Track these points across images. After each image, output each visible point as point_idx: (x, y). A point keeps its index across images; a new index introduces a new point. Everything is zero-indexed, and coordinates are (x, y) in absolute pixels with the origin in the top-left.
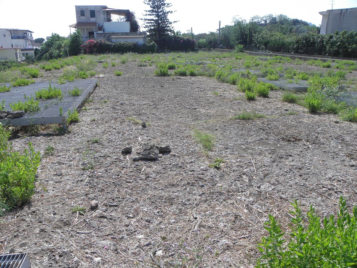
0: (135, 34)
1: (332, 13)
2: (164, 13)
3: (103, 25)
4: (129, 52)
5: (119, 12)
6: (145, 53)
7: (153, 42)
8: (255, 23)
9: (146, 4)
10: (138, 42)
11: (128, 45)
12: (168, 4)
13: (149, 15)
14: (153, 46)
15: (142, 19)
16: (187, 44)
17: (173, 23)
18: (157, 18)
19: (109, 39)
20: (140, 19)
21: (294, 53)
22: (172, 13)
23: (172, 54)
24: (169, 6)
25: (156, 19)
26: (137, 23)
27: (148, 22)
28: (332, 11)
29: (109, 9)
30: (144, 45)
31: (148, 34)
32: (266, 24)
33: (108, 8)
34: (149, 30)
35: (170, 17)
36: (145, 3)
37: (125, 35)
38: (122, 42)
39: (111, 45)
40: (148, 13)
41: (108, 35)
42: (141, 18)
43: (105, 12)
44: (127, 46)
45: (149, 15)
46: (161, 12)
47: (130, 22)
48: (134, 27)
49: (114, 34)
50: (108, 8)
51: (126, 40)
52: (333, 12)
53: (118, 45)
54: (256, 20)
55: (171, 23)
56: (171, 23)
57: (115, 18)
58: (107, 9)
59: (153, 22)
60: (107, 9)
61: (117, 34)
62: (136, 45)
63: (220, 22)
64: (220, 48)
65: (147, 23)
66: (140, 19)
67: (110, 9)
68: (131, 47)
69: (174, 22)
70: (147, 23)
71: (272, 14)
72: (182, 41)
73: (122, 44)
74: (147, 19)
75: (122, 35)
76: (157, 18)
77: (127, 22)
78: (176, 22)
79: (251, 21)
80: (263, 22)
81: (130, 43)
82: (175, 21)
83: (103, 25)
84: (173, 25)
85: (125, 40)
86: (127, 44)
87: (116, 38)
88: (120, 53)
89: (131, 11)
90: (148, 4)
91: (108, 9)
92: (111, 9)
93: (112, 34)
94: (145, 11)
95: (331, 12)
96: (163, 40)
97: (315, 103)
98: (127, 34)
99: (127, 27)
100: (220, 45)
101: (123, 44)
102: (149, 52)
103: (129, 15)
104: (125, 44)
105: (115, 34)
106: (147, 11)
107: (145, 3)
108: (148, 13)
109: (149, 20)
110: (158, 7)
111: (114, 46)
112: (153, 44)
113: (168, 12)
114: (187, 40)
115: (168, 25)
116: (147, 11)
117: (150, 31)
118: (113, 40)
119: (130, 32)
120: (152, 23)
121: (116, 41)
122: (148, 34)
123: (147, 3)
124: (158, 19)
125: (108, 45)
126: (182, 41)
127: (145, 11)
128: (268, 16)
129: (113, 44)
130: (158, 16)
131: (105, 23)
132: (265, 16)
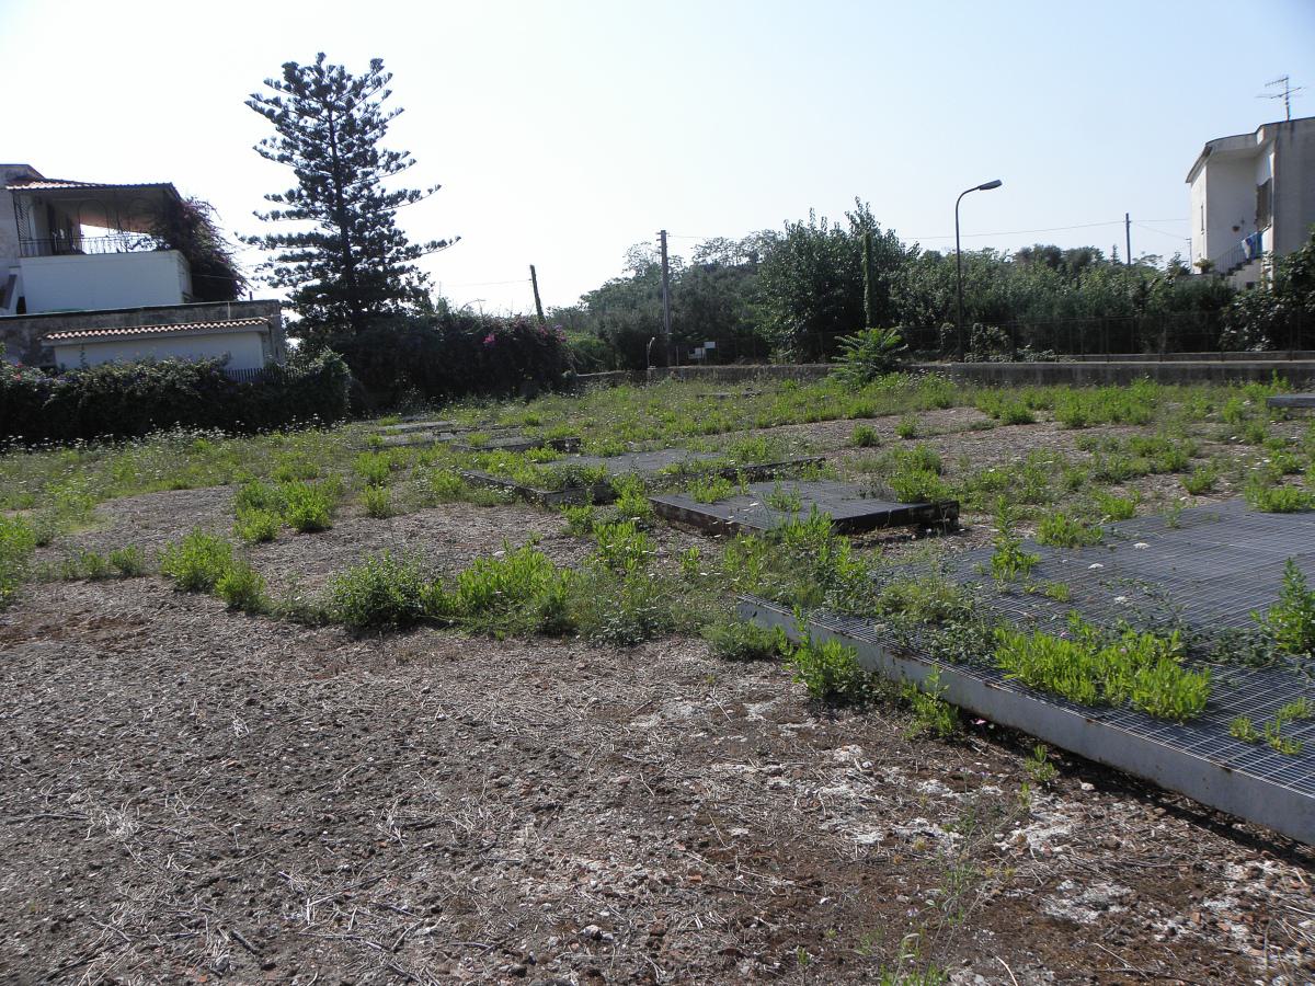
0: (212, 312)
1: (1292, 138)
2: (374, 203)
3: (13, 278)
4: (167, 426)
5: (117, 204)
6: (274, 427)
7: (327, 352)
8: (715, 266)
9: (272, 158)
10: (227, 358)
11: (157, 380)
12: (394, 157)
13: (290, 214)
14: (329, 374)
15: (253, 241)
16: (508, 360)
17: (424, 250)
18: (337, 230)
19: (38, 355)
20: (242, 239)
21: (1269, 347)
22: (417, 203)
23: (462, 417)
24: (399, 167)
25: (331, 233)
26: (228, 261)
27: (288, 252)
28: (1292, 129)
29: (50, 186)
30: (271, 377)
31: (294, 316)
32: (751, 268)
33: (46, 181)
34: (295, 298)
35: (405, 219)
36: (265, 155)
37: (146, 323)
38: (122, 363)
39: (44, 390)
40: (284, 207)
41: (33, 326)
42: (249, 235)
43: (26, 202)
44: (151, 389)
45: (290, 214)
46: (355, 198)
47: (186, 253)
48: (212, 278)
49: (70, 318)
50: (46, 181)
51: (151, 350)
52: (1300, 132)
53: (89, 388)
54: (719, 254)
55: (414, 252)
56: (414, 252)
57: (96, 238)
58: (34, 186)
59: (314, 250)
60: (34, 186)
61: (94, 318)
62: (214, 380)
63: (663, 233)
64: (703, 364)
65: (284, 259)
66: (242, 239)
67: (53, 181)
68: (183, 392)
69: (434, 245)
70: (284, 259)
71: (771, 229)
72: (490, 338)
73: (116, 380)
74: (281, 240)
75: (128, 325)
76: (337, 230)
77: (161, 253)
78: (443, 244)
79: (700, 260)
80: (745, 260)
81: (173, 367)
82: (438, 240)
83: (13, 278)
84: (422, 263)
85: (143, 352)
86: (151, 378)
87: (81, 345)
88: (106, 442)
89: (185, 193)
90: (282, 159)
91: (42, 186)
92: (62, 182)
93: (59, 321)
94: (267, 197)
95: (1285, 134)
96: (380, 349)
97: (180, 355)
98: (157, 314)
99: (168, 280)
100: (702, 346)
101: (129, 380)
102: (304, 415)
103: (166, 214)
104: (141, 375)
105: (81, 320)
106: (277, 198)
107: (265, 155)
108: (284, 207)
109: (290, 241)
110: (342, 173)
111: (63, 392)
112: (329, 364)
113: (394, 200)
114: (517, 329)
115: (396, 265)
116: (277, 198)
117: (303, 300)
118: (61, 358)
119: (185, 300)
120: (309, 257)
121: (82, 360)
122: (294, 316)
123: (276, 153)
124: (344, 232)
125: (22, 389)
126: (490, 338)
127: (267, 197)
128: (760, 238)
129: (59, 382)
130: (340, 216)
131: (23, 261)
132: (748, 239)
